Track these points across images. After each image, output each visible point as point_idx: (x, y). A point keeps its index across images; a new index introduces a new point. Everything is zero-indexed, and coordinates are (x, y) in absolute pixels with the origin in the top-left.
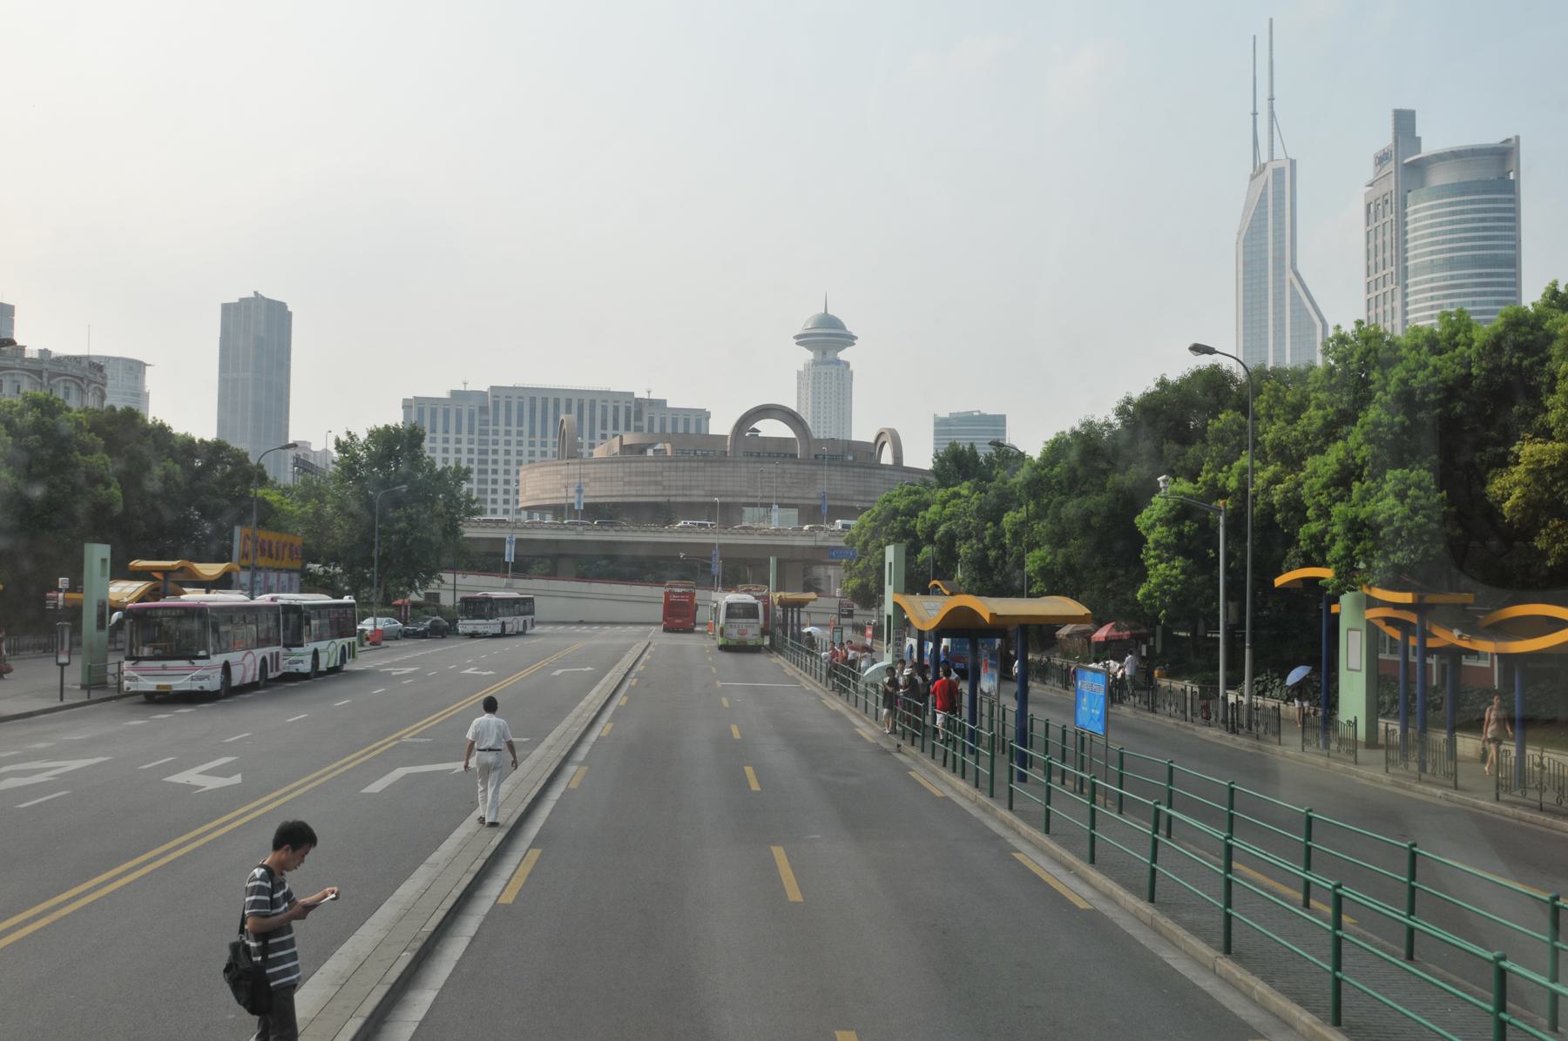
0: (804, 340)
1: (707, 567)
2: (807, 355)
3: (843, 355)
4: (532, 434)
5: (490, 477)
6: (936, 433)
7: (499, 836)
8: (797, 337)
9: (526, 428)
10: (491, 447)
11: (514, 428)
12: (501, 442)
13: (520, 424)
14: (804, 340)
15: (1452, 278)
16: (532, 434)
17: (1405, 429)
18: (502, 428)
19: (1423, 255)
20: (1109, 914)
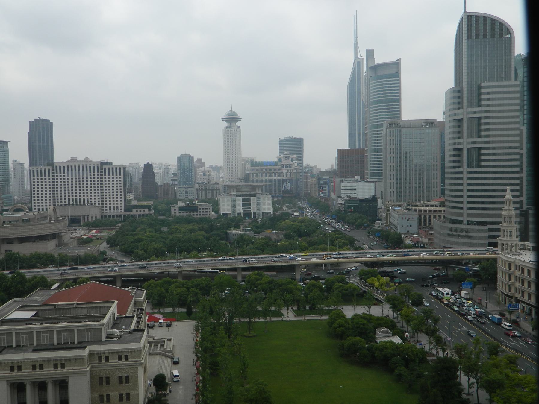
0: (224, 119)
1: (79, 222)
2: (226, 124)
3: (238, 124)
4: (68, 176)
5: (100, 197)
6: (280, 144)
7: (52, 347)
8: (223, 119)
9: (66, 174)
10: (56, 189)
11: (43, 178)
12: (107, 181)
13: (64, 173)
14: (224, 119)
15: (377, 107)
16: (68, 176)
17: (377, 328)
18: (107, 176)
19: (375, 98)
20: (466, 59)
